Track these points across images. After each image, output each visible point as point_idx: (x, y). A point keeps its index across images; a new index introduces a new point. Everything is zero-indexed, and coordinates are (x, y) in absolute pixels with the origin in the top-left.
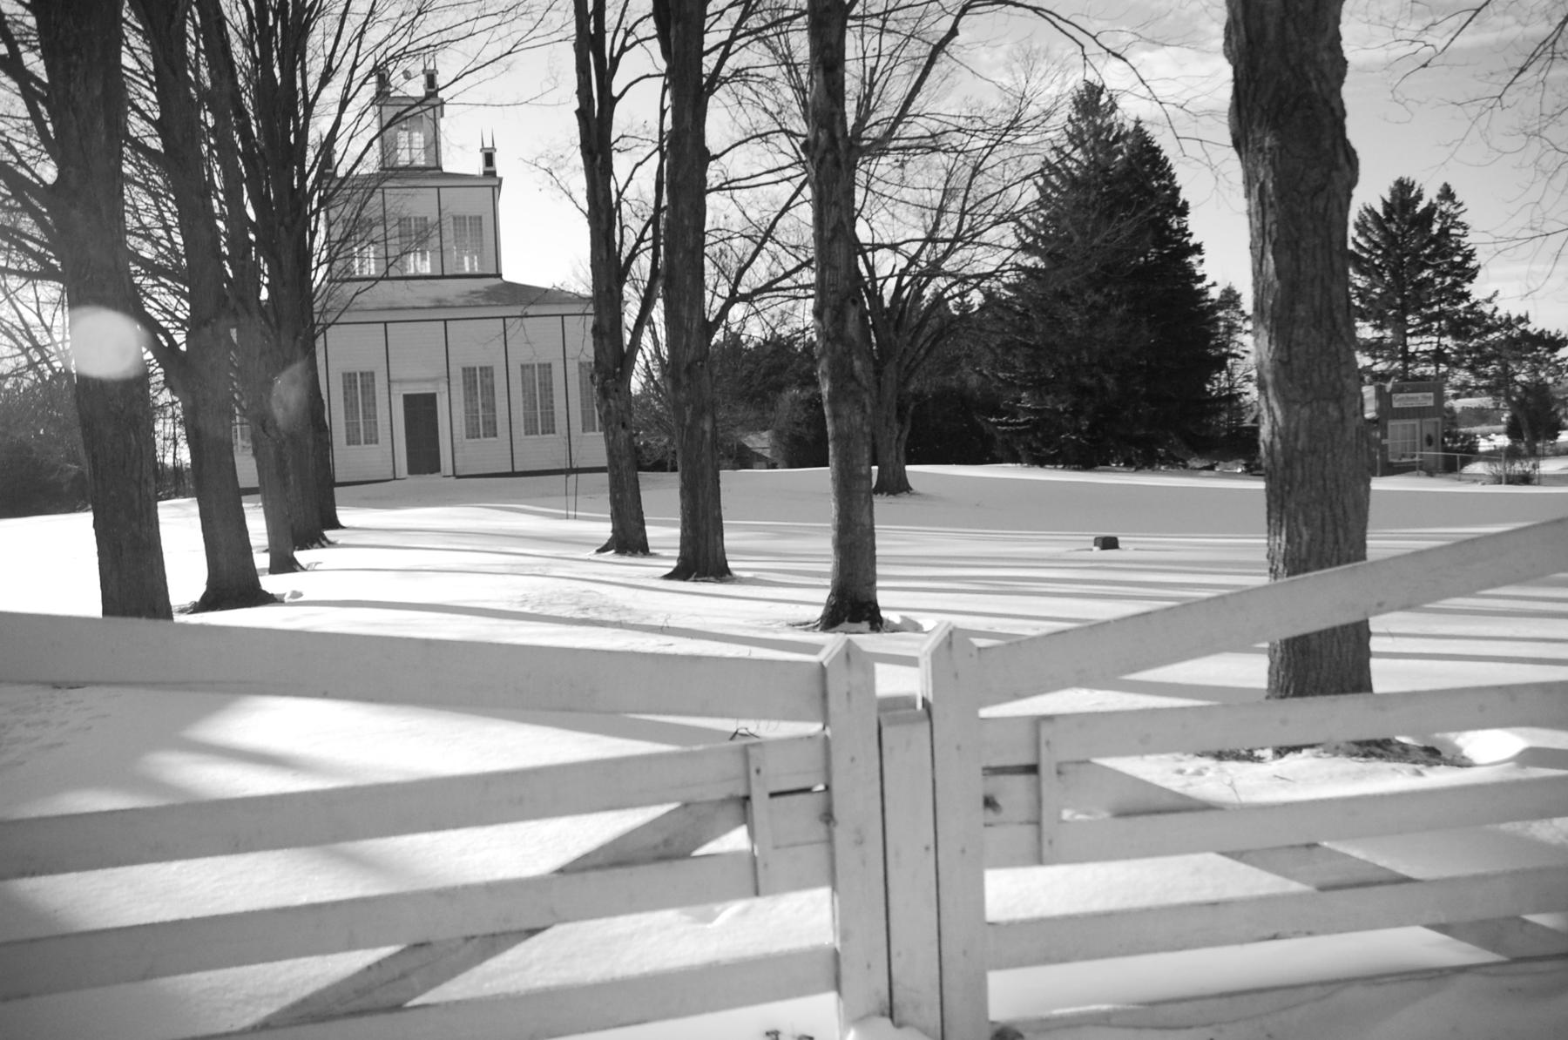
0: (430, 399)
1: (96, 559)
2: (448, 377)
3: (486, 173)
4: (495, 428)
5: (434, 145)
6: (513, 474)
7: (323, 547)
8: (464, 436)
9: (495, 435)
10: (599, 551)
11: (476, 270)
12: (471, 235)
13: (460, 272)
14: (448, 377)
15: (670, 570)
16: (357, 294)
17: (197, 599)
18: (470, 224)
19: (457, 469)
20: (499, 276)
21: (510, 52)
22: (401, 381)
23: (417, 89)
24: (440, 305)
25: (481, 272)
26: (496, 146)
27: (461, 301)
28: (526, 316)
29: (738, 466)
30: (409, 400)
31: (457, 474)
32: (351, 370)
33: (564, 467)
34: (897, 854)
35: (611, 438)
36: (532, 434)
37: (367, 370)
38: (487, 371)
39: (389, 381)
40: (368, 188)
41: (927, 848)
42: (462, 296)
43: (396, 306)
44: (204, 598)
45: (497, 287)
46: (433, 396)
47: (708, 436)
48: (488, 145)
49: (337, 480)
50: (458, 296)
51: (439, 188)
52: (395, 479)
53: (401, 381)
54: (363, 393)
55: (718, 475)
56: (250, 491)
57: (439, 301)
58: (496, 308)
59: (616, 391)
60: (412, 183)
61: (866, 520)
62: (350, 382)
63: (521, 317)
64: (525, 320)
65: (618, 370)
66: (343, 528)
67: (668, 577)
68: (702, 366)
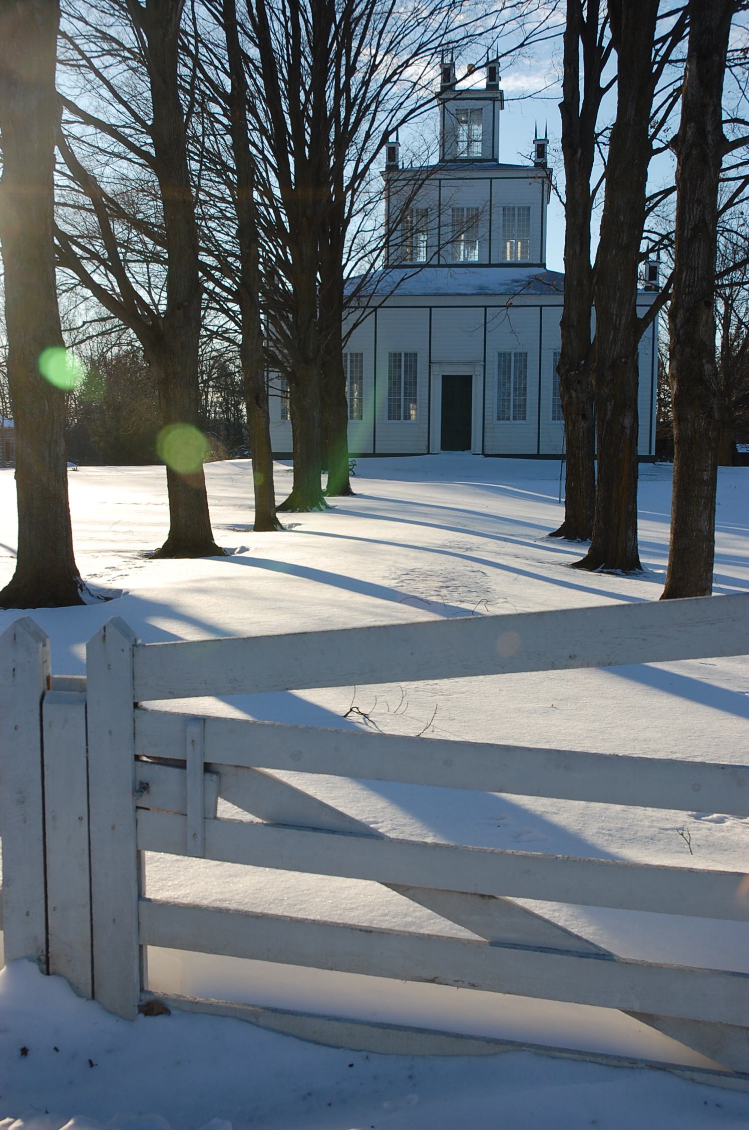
0: (466, 381)
1: (70, 506)
2: (485, 361)
3: (537, 165)
4: (525, 411)
5: (492, 138)
6: (538, 456)
7: (321, 510)
8: (495, 417)
9: (524, 418)
10: (551, 535)
11: (508, 259)
12: (519, 226)
13: (504, 262)
14: (485, 361)
15: (579, 559)
16: (403, 280)
17: (160, 545)
18: (519, 215)
19: (486, 448)
20: (544, 265)
21: (522, 45)
22: (440, 363)
23: (479, 81)
24: (482, 292)
25: (525, 261)
26: (400, 141)
27: (502, 289)
28: (511, 306)
29: (227, 457)
30: (447, 381)
31: (486, 452)
32: (397, 351)
33: (560, 453)
34: (54, 819)
35: (570, 428)
36: (394, 419)
37: (410, 351)
38: (522, 357)
39: (430, 362)
40: (418, 179)
41: (81, 819)
42: (505, 284)
43: (440, 292)
44: (166, 544)
45: (536, 278)
46: (469, 378)
47: (628, 431)
48: (541, 136)
49: (372, 452)
50: (501, 284)
51: (491, 179)
52: (429, 453)
53: (440, 363)
54: (406, 372)
55: (716, 469)
56: (282, 457)
57: (481, 288)
58: (533, 297)
59: (579, 382)
60: (462, 175)
61: (704, 525)
62: (395, 362)
63: (507, 307)
64: (510, 310)
65: (583, 362)
66: (353, 495)
67: (576, 565)
68: (626, 362)
